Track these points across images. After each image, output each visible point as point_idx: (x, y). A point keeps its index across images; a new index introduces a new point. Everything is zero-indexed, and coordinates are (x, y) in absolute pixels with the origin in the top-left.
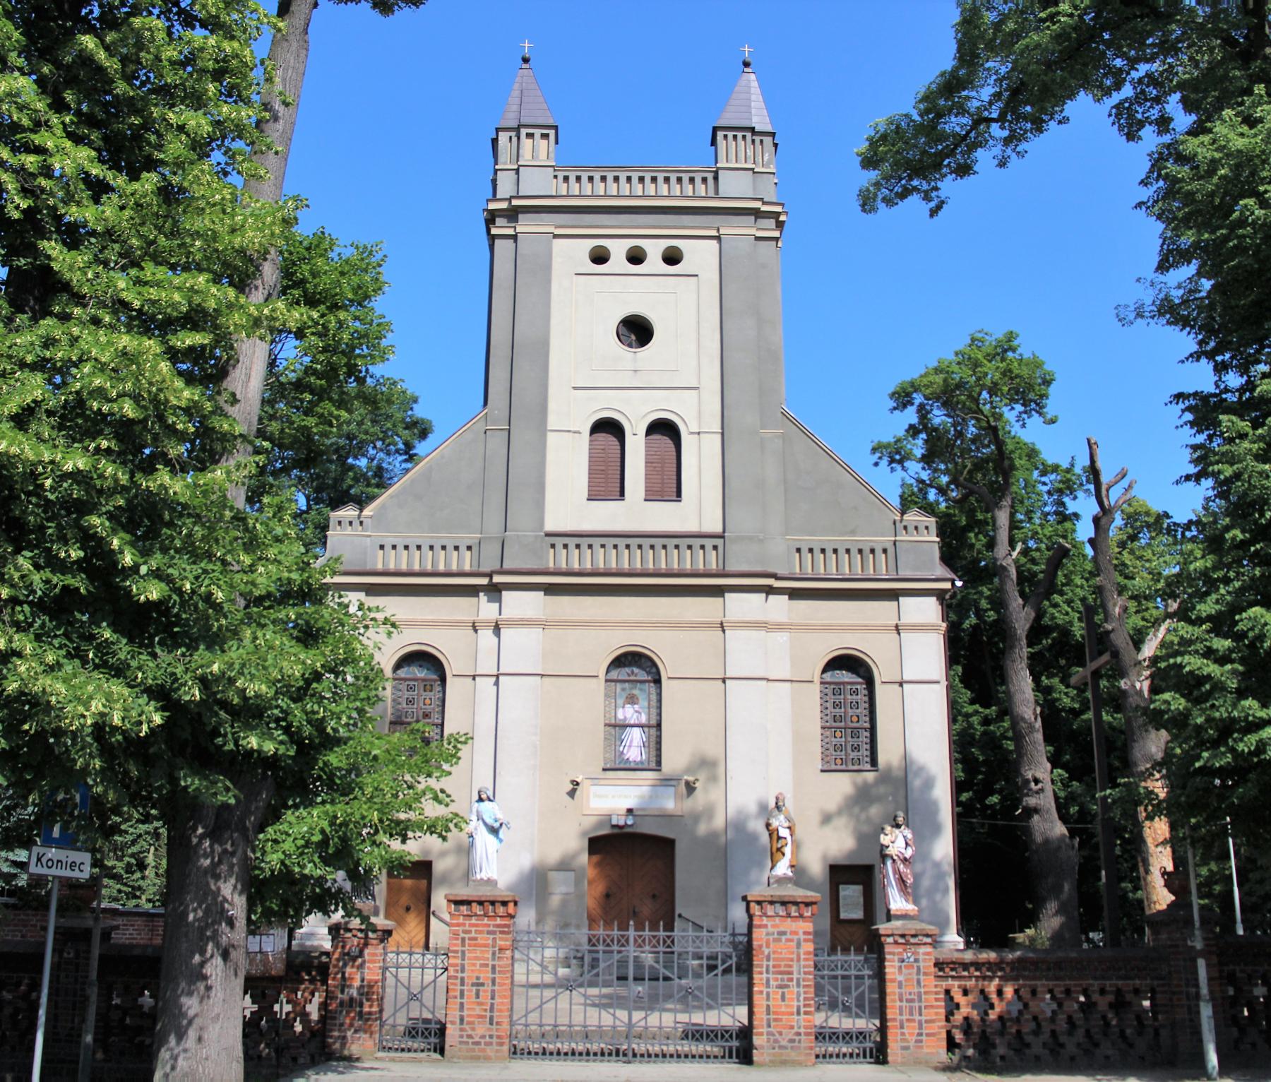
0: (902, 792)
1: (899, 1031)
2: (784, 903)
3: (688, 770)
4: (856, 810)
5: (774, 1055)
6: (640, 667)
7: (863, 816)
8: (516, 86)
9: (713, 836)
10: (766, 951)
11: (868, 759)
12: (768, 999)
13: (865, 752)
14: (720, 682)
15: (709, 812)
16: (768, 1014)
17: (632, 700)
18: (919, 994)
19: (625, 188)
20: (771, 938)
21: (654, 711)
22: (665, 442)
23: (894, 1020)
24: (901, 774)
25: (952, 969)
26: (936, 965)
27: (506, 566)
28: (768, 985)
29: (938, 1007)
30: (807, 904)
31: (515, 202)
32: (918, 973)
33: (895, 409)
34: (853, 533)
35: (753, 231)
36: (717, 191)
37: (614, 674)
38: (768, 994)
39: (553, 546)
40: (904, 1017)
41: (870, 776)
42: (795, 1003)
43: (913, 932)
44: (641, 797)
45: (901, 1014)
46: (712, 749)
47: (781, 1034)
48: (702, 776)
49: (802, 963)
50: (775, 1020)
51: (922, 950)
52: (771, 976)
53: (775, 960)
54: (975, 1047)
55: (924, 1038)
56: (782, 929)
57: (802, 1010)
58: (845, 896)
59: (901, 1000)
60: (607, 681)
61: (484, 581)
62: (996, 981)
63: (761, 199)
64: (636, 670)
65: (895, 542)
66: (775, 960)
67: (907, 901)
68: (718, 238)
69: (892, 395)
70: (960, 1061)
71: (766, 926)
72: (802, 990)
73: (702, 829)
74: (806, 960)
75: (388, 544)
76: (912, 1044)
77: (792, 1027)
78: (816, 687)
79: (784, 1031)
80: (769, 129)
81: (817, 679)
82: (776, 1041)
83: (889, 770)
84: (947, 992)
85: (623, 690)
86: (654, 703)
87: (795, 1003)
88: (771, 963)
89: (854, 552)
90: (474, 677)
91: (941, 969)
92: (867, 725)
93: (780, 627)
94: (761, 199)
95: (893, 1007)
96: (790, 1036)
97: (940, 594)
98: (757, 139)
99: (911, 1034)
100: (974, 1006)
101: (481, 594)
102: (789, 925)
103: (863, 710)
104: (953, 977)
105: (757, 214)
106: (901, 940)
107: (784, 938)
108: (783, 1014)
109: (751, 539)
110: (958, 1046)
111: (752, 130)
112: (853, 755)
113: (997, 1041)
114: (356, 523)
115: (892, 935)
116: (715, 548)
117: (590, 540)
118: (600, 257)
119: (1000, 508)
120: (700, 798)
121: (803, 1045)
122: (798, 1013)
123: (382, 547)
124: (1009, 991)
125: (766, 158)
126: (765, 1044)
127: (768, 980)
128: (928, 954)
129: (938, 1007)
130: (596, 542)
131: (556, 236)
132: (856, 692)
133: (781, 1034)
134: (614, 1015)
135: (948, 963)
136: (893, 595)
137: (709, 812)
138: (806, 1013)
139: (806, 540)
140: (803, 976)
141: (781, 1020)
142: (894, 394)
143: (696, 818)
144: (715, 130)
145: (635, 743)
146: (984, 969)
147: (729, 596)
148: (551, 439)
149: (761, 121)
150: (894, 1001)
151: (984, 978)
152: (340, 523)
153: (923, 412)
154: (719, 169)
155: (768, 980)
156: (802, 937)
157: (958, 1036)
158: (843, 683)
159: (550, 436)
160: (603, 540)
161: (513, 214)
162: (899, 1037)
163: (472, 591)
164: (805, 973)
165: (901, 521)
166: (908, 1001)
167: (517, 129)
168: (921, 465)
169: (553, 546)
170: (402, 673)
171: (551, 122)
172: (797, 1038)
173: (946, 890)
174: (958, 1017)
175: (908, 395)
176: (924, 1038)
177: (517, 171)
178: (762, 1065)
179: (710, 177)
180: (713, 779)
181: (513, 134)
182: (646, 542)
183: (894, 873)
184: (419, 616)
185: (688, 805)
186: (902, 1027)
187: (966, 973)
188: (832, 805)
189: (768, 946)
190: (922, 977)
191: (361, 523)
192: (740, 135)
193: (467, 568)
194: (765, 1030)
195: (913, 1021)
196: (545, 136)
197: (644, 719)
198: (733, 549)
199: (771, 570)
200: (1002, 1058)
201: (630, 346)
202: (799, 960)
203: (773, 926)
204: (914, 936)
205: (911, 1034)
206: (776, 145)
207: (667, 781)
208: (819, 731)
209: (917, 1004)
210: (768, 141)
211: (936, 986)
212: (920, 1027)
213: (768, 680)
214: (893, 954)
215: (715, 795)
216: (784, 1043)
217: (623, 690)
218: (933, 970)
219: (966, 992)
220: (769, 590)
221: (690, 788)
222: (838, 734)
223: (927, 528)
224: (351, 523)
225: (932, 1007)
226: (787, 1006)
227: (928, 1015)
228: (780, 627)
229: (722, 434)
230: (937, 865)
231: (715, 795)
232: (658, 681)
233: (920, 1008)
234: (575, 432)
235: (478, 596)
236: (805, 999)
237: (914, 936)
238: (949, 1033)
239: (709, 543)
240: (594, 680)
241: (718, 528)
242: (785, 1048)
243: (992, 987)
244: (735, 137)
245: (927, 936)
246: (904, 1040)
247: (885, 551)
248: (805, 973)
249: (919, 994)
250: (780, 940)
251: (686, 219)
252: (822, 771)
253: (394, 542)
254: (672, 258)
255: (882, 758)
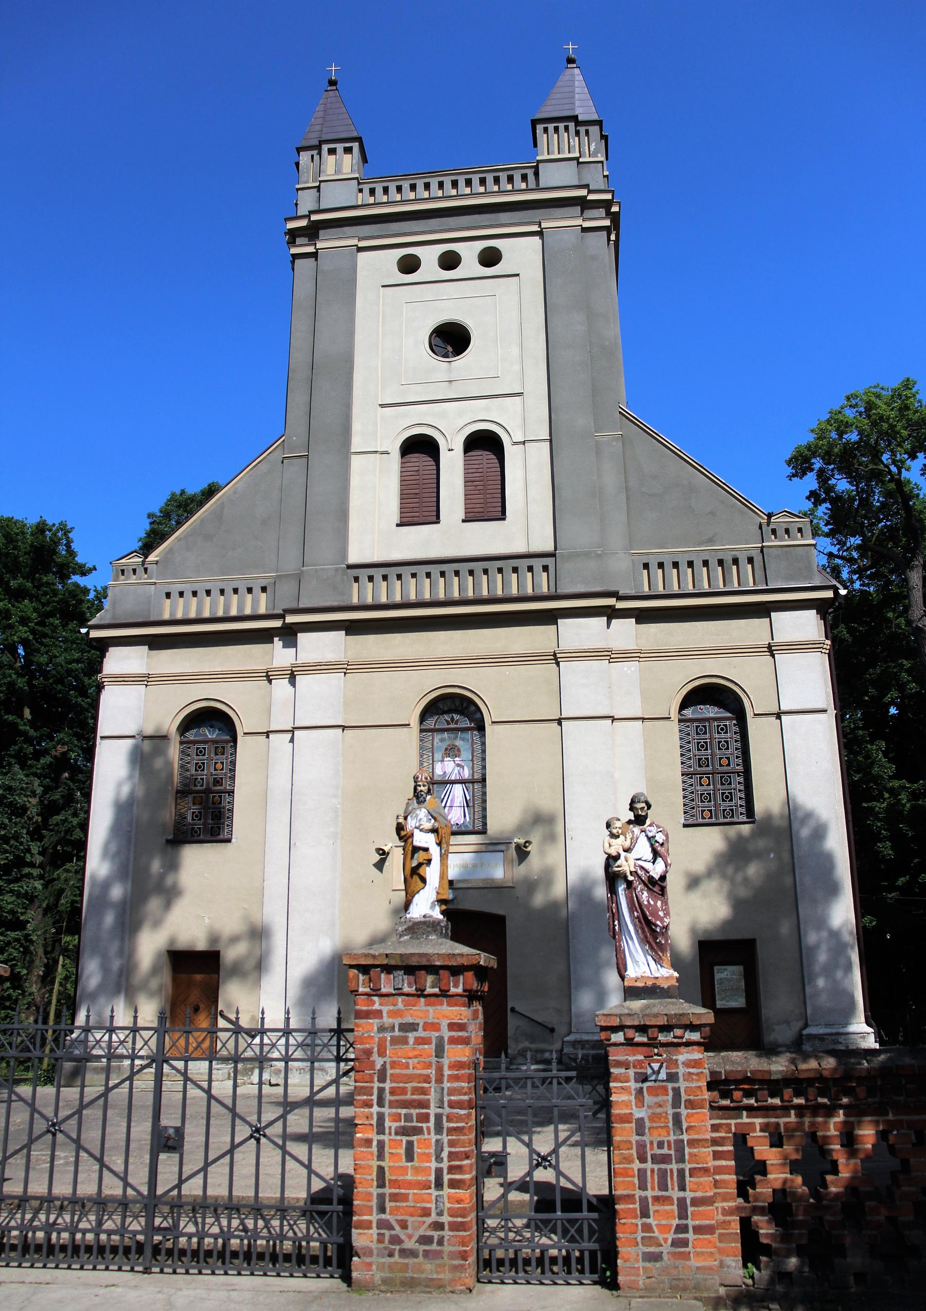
0: (787, 846)
1: (639, 1222)
2: (410, 970)
3: (521, 829)
4: (730, 870)
5: (391, 1268)
6: (461, 713)
7: (739, 877)
8: (320, 108)
9: (553, 907)
10: (379, 1062)
11: (743, 810)
12: (381, 1156)
13: (739, 800)
14: (555, 724)
15: (547, 878)
16: (381, 1185)
17: (452, 751)
18: (679, 1146)
19: (436, 192)
20: (388, 1035)
21: (478, 763)
22: (486, 457)
23: (630, 1198)
24: (785, 823)
25: (748, 1094)
26: (711, 1086)
27: (323, 206)
28: (381, 1129)
29: (719, 1170)
30: (456, 971)
31: (314, 217)
32: (676, 1103)
33: (794, 475)
34: (711, 541)
35: (579, 222)
36: (538, 184)
37: (430, 723)
38: (381, 1145)
39: (356, 579)
40: (649, 1193)
41: (746, 829)
42: (433, 1165)
43: (662, 1021)
44: (465, 866)
45: (643, 1187)
46: (547, 803)
47: (404, 1225)
48: (536, 838)
49: (447, 1085)
50: (394, 1197)
51: (684, 1056)
52: (386, 1110)
53: (394, 1078)
54: (800, 1252)
55: (690, 1236)
56: (409, 1019)
57: (446, 1177)
58: (721, 981)
59: (643, 1159)
60: (422, 731)
61: (277, 624)
62: (840, 1117)
63: (586, 186)
64: (457, 717)
65: (762, 547)
66: (394, 1078)
67: (658, 961)
68: (540, 234)
69: (789, 463)
70: (771, 1282)
71: (378, 1014)
72: (445, 1138)
73: (539, 900)
74: (452, 1078)
75: (175, 589)
76: (666, 1249)
77: (426, 1213)
78: (674, 727)
79: (410, 1219)
80: (595, 117)
81: (674, 715)
82: (396, 1240)
83: (769, 817)
84: (741, 1139)
85: (442, 740)
86: (478, 753)
87: (433, 1165)
88: (388, 1085)
89: (713, 563)
90: (267, 734)
91: (725, 1095)
92: (740, 768)
93: (625, 656)
94: (586, 186)
95: (626, 1173)
96: (422, 1232)
97: (820, 606)
98: (582, 130)
99: (664, 1228)
100: (795, 1167)
101: (276, 639)
102: (422, 1012)
103: (734, 749)
104: (750, 1109)
105: (583, 204)
106: (639, 1039)
107: (411, 1036)
108: (410, 1185)
109: (587, 555)
110: (767, 1250)
111: (575, 118)
112: (724, 805)
113: (848, 1241)
114: (140, 570)
115: (620, 1028)
116: (545, 568)
117: (399, 570)
118: (409, 265)
119: (912, 568)
120: (535, 863)
121: (447, 1248)
122: (439, 1185)
123: (168, 595)
124: (867, 1133)
125: (593, 148)
126: (374, 1246)
127: (381, 1117)
128: (696, 1063)
129: (719, 1170)
130: (406, 571)
131: (360, 249)
132: (725, 730)
133: (404, 1225)
134: (126, 1184)
135: (737, 1082)
136: (763, 611)
137: (547, 878)
138: (453, 1184)
139: (655, 553)
140: (447, 1110)
141: (405, 1198)
142: (791, 460)
143: (531, 885)
144: (534, 123)
145: (457, 803)
146: (812, 1091)
147: (565, 624)
148: (356, 462)
149: (585, 110)
150: (628, 1160)
151: (816, 1109)
152: (123, 571)
153: (822, 477)
154: (539, 162)
155: (381, 1117)
156: (446, 1034)
157: (766, 1229)
158: (708, 720)
159: (356, 461)
160: (413, 569)
161: (313, 231)
162: (640, 1235)
163: (265, 636)
164: (452, 1105)
165: (768, 524)
166: (656, 1159)
167: (318, 148)
168: (828, 540)
169: (356, 579)
170: (191, 735)
171: (355, 134)
172: (436, 1234)
173: (849, 967)
174: (764, 1190)
175: (807, 460)
176: (690, 1236)
177: (318, 188)
178: (367, 1287)
179: (530, 173)
180: (551, 838)
181: (315, 152)
182: (464, 568)
183: (631, 909)
184: (206, 668)
185: (521, 871)
186: (645, 1214)
187: (777, 1101)
188: (699, 865)
189: (382, 1053)
190: (684, 1112)
191: (146, 570)
192: (561, 126)
193: (262, 610)
194: (374, 1218)
195: (668, 1200)
196: (348, 150)
197: (466, 774)
198: (566, 567)
199: (613, 588)
200: (860, 1277)
201: (446, 356)
202: (439, 1080)
203: (392, 1014)
204: (666, 1028)
205: (664, 1228)
206: (604, 138)
207: (495, 846)
208: (680, 778)
209: (674, 1166)
210: (594, 130)
211: (715, 1128)
212: (683, 1215)
213: (613, 719)
214: (626, 1065)
215: (553, 857)
216: (410, 1244)
217: (442, 740)
218: (707, 1095)
219: (777, 1141)
220: (611, 614)
221: (522, 853)
222: (705, 780)
223: (800, 530)
224: (134, 571)
225: (706, 1171)
226: (416, 1170)
227: (698, 1188)
228: (625, 656)
229: (551, 441)
230: (835, 935)
231: (553, 857)
232: (481, 728)
233: (681, 1172)
234: (383, 453)
235: (272, 642)
236: (451, 1156)
237: (666, 1028)
238: (745, 1223)
239: (537, 564)
240: (405, 730)
241: (549, 547)
242: (413, 1254)
243: (833, 1126)
244: (556, 129)
245: (692, 1027)
246: (647, 1241)
247: (750, 560)
248: (452, 1105)
249: (679, 1146)
250: (405, 1041)
251: (504, 217)
252: (685, 826)
253: (181, 587)
254: (490, 258)
255: (759, 807)
